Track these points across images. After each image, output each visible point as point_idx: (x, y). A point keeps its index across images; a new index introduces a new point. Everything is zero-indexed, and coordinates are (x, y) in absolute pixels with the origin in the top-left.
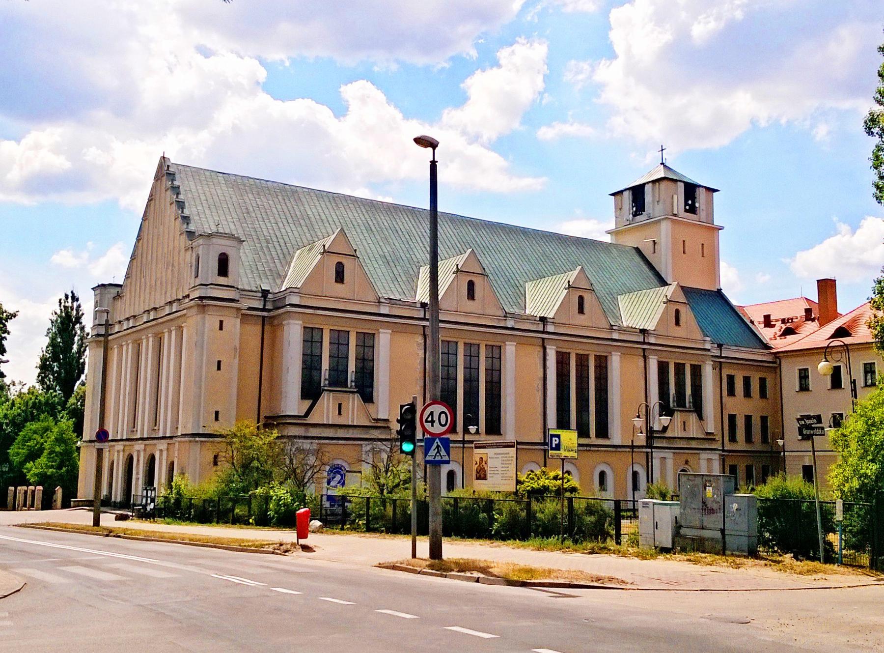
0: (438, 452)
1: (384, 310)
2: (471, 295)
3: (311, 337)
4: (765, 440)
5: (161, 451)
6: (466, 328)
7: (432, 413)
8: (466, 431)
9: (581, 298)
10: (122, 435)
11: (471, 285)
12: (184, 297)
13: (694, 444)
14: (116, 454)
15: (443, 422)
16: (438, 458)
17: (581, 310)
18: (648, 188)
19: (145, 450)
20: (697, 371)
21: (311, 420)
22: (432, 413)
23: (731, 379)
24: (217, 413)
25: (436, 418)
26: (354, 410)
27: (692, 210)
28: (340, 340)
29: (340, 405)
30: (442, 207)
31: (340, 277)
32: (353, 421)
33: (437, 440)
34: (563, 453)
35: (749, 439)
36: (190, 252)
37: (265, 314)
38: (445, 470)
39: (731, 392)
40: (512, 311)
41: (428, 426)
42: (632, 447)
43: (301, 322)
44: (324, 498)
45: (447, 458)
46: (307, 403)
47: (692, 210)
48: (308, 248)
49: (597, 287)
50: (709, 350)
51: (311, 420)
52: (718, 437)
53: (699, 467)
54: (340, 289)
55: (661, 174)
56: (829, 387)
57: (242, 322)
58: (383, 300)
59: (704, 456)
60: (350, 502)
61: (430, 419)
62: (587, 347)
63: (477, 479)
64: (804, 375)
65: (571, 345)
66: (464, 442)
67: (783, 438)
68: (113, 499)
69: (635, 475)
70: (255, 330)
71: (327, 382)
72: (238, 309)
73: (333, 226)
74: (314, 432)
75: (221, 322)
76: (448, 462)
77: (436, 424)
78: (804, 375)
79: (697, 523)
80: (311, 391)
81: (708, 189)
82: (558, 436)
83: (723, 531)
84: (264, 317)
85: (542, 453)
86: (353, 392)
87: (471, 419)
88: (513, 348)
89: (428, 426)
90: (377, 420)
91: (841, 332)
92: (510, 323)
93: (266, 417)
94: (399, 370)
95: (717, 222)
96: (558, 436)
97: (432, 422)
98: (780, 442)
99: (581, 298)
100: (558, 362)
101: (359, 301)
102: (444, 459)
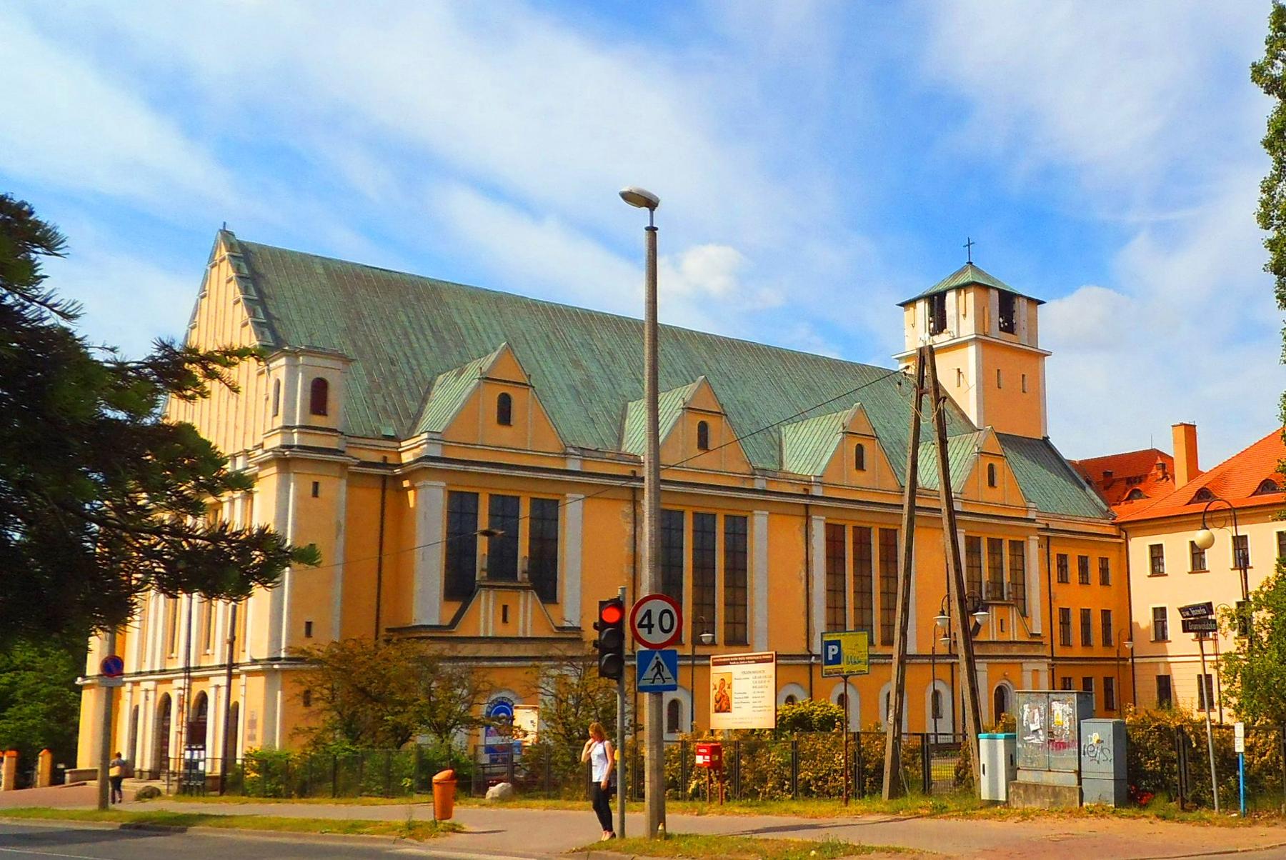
0: (659, 672)
1: (573, 465)
2: (703, 443)
3: (460, 509)
4: (1107, 641)
5: (218, 687)
6: (697, 491)
7: (649, 613)
8: (697, 641)
9: (860, 449)
10: (153, 664)
11: (703, 428)
12: (257, 447)
13: (1015, 651)
14: (143, 694)
15: (667, 627)
16: (658, 682)
17: (860, 465)
18: (951, 297)
19: (155, 690)
20: (1018, 547)
21: (460, 632)
22: (649, 613)
23: (1062, 558)
24: (309, 625)
25: (655, 620)
26: (527, 616)
27: (1009, 327)
28: (505, 509)
29: (505, 608)
30: (662, 319)
31: (504, 416)
32: (525, 632)
33: (657, 654)
34: (845, 667)
35: (1086, 642)
36: (264, 377)
37: (387, 472)
38: (668, 697)
39: (1063, 579)
40: (760, 466)
41: (643, 632)
42: (934, 656)
43: (444, 484)
44: (481, 750)
45: (671, 682)
46: (456, 606)
47: (1009, 327)
48: (455, 372)
49: (882, 434)
50: (1033, 520)
51: (460, 632)
52: (1047, 641)
53: (1021, 682)
54: (505, 435)
55: (968, 277)
56: (1232, 566)
57: (349, 485)
58: (572, 451)
59: (1029, 666)
60: (869, 762)
61: (645, 622)
62: (868, 518)
63: (717, 711)
64: (1156, 553)
65: (847, 516)
66: (694, 657)
67: (1131, 639)
68: (138, 766)
69: (936, 694)
70: (371, 498)
71: (485, 574)
72: (344, 466)
73: (495, 341)
74: (467, 650)
75: (316, 485)
76: (674, 688)
77: (656, 629)
78: (1156, 553)
79: (1043, 764)
80: (460, 587)
81: (1030, 300)
82: (838, 643)
83: (1079, 773)
84: (384, 477)
85: (949, 668)
86: (525, 589)
87: (704, 622)
88: (765, 520)
89: (643, 632)
90: (562, 629)
91: (1203, 494)
92: (759, 484)
93: (388, 630)
94: (599, 556)
95: (1042, 346)
96: (838, 643)
97: (650, 626)
98: (1128, 645)
99: (860, 449)
100: (828, 540)
101: (533, 453)
102: (668, 683)
